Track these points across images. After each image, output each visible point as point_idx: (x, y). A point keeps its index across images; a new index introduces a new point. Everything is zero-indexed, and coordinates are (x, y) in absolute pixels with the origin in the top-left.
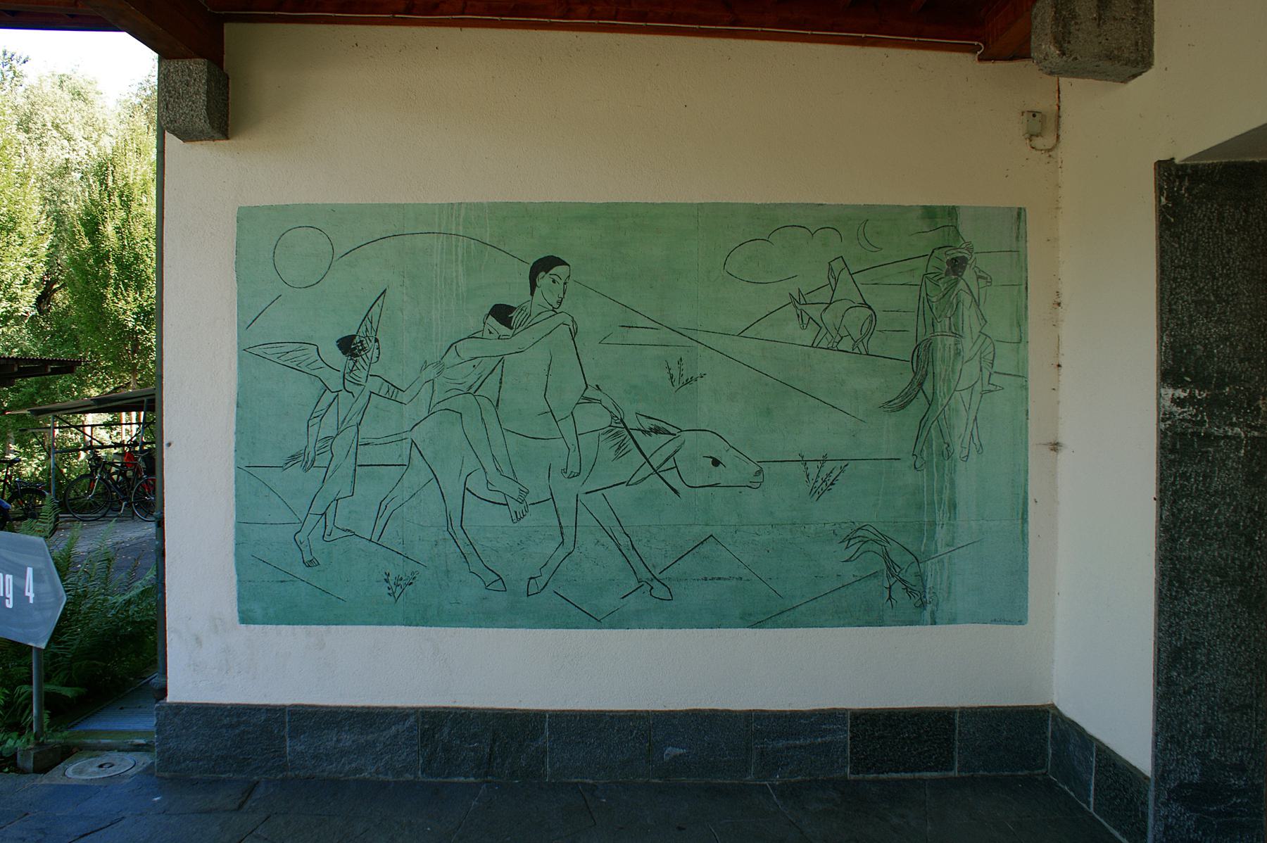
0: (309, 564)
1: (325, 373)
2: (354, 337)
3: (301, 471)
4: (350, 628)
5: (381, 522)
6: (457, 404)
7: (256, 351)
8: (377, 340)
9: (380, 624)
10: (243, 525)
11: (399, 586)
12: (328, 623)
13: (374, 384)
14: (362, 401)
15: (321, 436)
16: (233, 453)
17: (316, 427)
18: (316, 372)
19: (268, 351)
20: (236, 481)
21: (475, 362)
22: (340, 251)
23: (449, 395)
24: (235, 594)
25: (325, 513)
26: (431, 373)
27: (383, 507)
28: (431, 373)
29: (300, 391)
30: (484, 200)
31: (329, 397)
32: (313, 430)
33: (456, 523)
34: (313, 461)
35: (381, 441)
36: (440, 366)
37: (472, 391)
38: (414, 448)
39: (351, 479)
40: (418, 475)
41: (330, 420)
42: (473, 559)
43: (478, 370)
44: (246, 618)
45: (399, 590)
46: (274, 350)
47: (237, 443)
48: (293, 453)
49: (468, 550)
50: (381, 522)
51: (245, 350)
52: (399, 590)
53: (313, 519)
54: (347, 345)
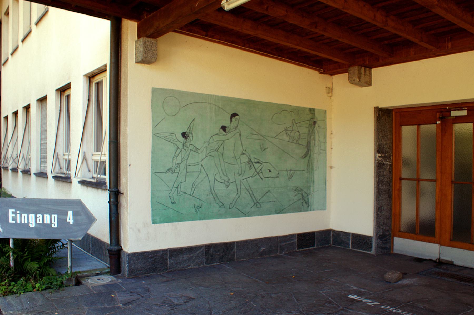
1: (178, 143)
5: (193, 189)
7: (158, 135)
13: (191, 147)
14: (188, 152)
15: (177, 163)
18: (176, 143)
25: (177, 187)
26: (206, 144)
28: (206, 144)
29: (170, 149)
31: (179, 151)
32: (174, 161)
33: (212, 189)
40: (203, 175)
42: (216, 199)
44: (154, 222)
48: (169, 168)
49: (215, 196)
50: (193, 189)
51: (155, 135)
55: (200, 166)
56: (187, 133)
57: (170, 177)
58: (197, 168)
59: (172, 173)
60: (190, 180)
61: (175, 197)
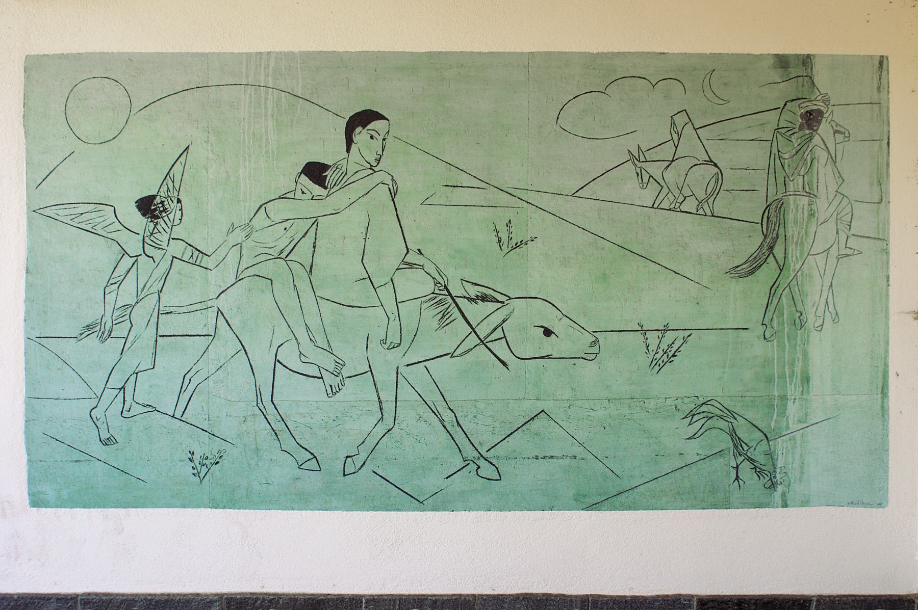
0: (106, 443)
1: (124, 237)
2: (154, 197)
3: (97, 341)
5: (185, 397)
7: (47, 212)
8: (179, 201)
9: (184, 506)
10: (33, 399)
11: (202, 466)
12: (127, 505)
13: (177, 248)
14: (164, 266)
17: (114, 295)
19: (60, 212)
20: (25, 353)
22: (138, 104)
23: (259, 259)
24: (25, 475)
25: (123, 388)
26: (238, 236)
27: (187, 381)
29: (96, 256)
30: (296, 49)
31: (127, 262)
32: (110, 298)
33: (266, 397)
34: (111, 332)
36: (249, 229)
37: (283, 255)
40: (226, 345)
41: (129, 286)
43: (289, 234)
44: (37, 501)
45: (204, 470)
46: (67, 212)
47: (28, 312)
50: (185, 397)
51: (36, 211)
52: (204, 470)
53: (110, 394)
54: (146, 206)
55: (212, 313)
56: (158, 200)
57: (98, 355)
58: (202, 322)
60: (173, 363)
61: (116, 422)
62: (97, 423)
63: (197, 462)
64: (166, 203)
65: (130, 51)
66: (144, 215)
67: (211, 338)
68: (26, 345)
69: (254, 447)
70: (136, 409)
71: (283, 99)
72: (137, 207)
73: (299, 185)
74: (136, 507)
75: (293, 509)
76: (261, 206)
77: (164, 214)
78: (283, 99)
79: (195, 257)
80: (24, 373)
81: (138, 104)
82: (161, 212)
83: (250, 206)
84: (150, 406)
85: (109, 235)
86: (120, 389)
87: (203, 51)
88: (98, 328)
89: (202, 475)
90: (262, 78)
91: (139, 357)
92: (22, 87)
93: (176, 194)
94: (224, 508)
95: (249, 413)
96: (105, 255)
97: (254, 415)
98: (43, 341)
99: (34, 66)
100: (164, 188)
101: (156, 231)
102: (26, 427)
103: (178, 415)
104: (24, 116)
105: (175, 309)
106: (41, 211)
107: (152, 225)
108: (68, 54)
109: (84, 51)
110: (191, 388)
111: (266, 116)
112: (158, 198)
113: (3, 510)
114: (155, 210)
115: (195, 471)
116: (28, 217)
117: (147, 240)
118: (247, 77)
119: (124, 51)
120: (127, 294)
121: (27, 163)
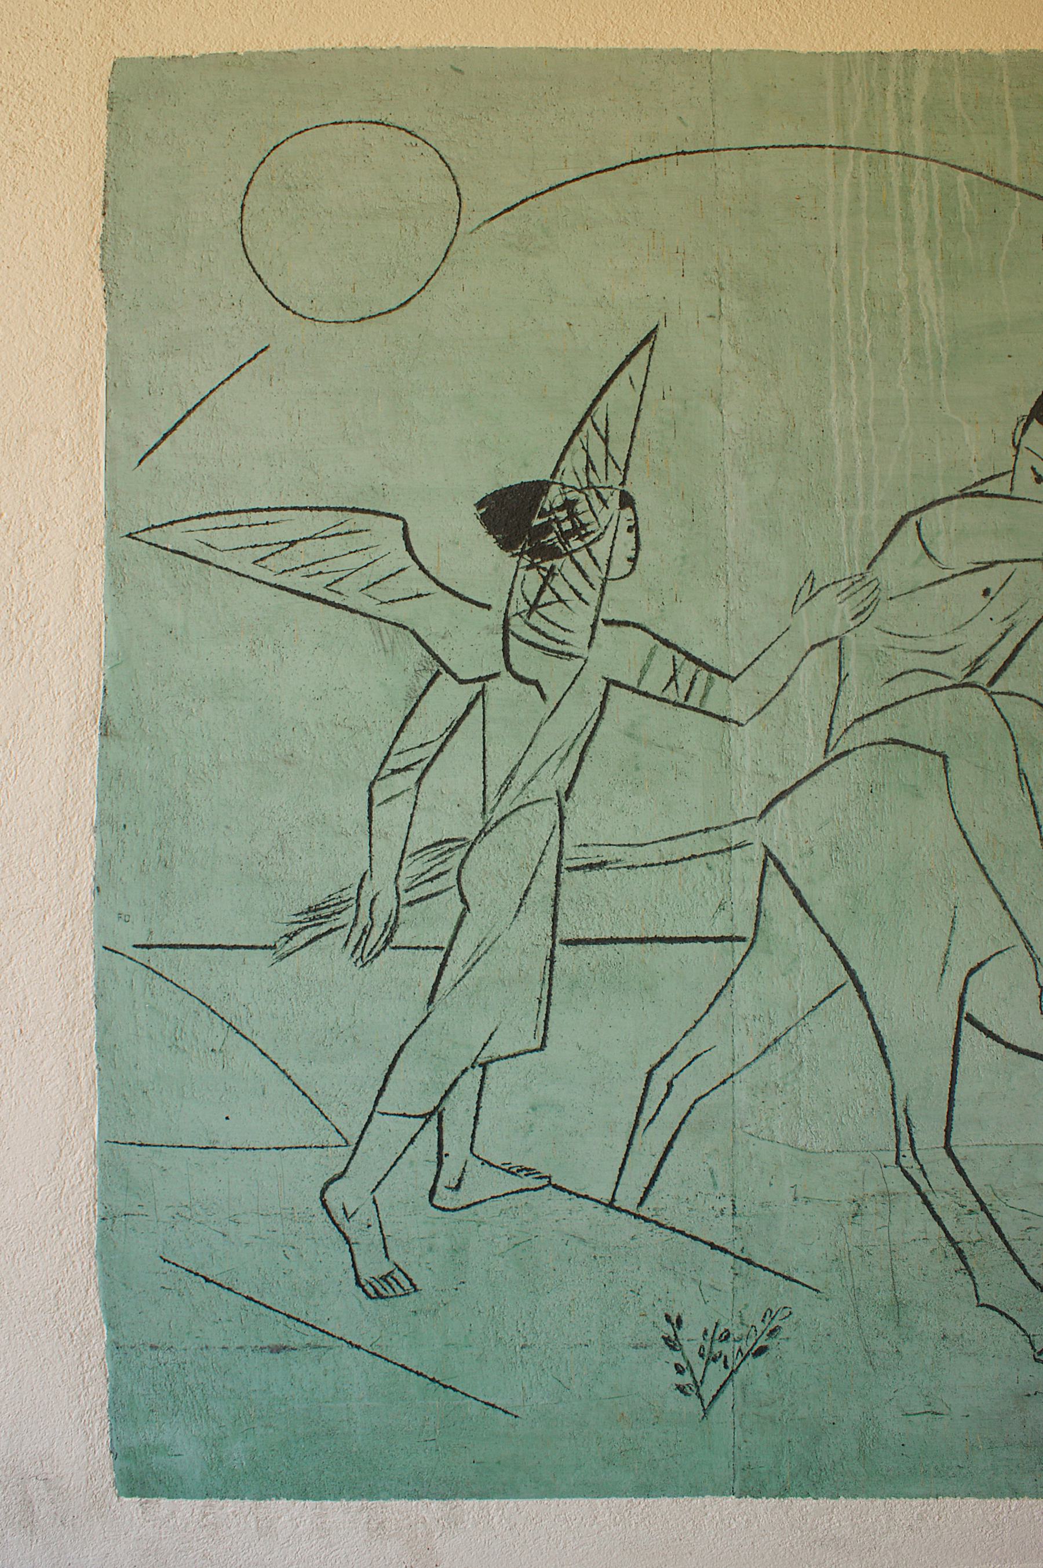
0: (378, 1289)
1: (435, 616)
2: (540, 488)
3: (344, 960)
4: (529, 1506)
5: (654, 1140)
6: (927, 721)
7: (174, 537)
8: (627, 501)
9: (646, 1491)
10: (123, 1149)
11: (712, 1362)
12: (450, 1489)
13: (619, 654)
14: (576, 714)
15: (421, 837)
16: (87, 896)
17: (402, 808)
18: (399, 612)
19: (220, 539)
20: (100, 997)
21: (991, 578)
22: (482, 201)
23: (900, 689)
24: (99, 1392)
25: (437, 1113)
26: (831, 613)
27: (658, 1088)
28: (831, 613)
29: (337, 680)
30: (995, 45)
31: (448, 698)
32: (391, 818)
33: (929, 1136)
34: (392, 927)
35: (651, 854)
36: (866, 593)
37: (982, 677)
38: (774, 878)
39: (537, 989)
40: (792, 970)
41: (457, 780)
42: (990, 1258)
43: (999, 608)
44: (141, 1476)
45: (716, 1373)
46: (241, 537)
47: (105, 865)
48: (316, 895)
49: (970, 1228)
50: (654, 1140)
51: (137, 538)
52: (716, 1373)
53: (389, 1133)
54: (516, 517)
55: (745, 868)
56: (554, 496)
57: (361, 1001)
58: (694, 899)
59: (364, 956)
60: (608, 1033)
61: (412, 1226)
62: (346, 1226)
63: (691, 1350)
64: (580, 507)
65: (454, 43)
66: (506, 545)
67: (742, 947)
68: (99, 971)
69: (885, 1297)
70: (483, 1183)
71: (962, 192)
72: (484, 519)
73: (1023, 453)
74: (481, 1496)
75: (1016, 1494)
76: (904, 519)
77: (575, 543)
78: (962, 192)
79: (683, 681)
80: (94, 1061)
81: (482, 201)
82: (565, 536)
83: (867, 519)
84: (529, 1172)
85: (386, 612)
86: (427, 1117)
87: (694, 45)
88: (347, 917)
89: (707, 1393)
90: (892, 127)
91: (490, 1011)
92: (100, 153)
93: (616, 478)
94: (783, 1493)
95: (871, 1188)
96: (367, 677)
97: (887, 1195)
98: (159, 959)
99: (141, 94)
100: (576, 460)
101: (547, 596)
102: (103, 1237)
103: (628, 1197)
104: (104, 240)
105: (617, 853)
106: (155, 536)
107: (533, 580)
108: (250, 55)
109: (305, 45)
110: (673, 1111)
111: (908, 240)
112: (555, 490)
113: (28, 1503)
114: (546, 528)
115: (686, 1379)
116: (111, 556)
117: (517, 625)
118: (842, 124)
119: (436, 43)
120: (450, 802)
121: (111, 386)
